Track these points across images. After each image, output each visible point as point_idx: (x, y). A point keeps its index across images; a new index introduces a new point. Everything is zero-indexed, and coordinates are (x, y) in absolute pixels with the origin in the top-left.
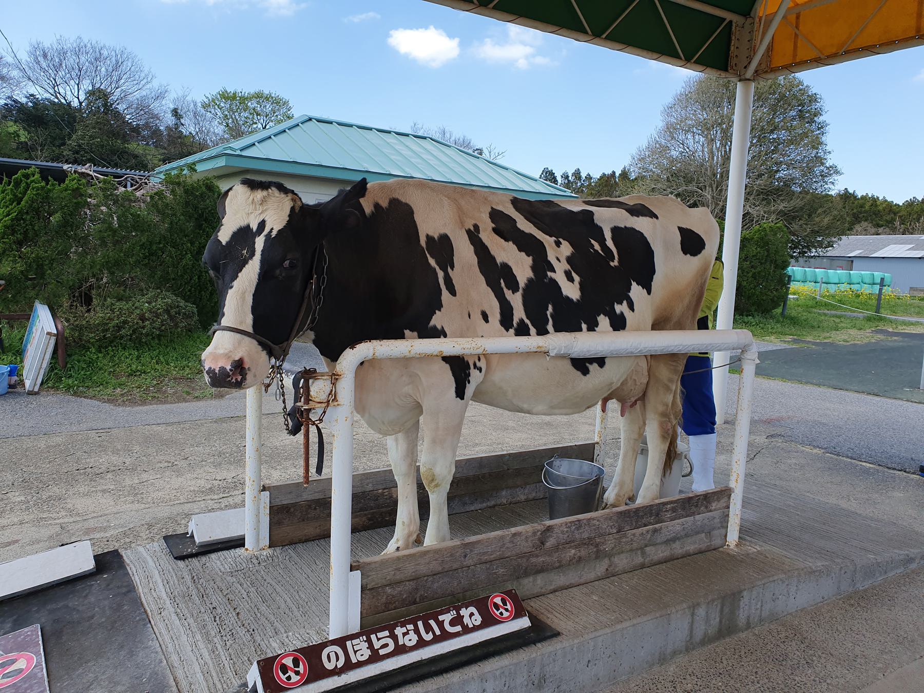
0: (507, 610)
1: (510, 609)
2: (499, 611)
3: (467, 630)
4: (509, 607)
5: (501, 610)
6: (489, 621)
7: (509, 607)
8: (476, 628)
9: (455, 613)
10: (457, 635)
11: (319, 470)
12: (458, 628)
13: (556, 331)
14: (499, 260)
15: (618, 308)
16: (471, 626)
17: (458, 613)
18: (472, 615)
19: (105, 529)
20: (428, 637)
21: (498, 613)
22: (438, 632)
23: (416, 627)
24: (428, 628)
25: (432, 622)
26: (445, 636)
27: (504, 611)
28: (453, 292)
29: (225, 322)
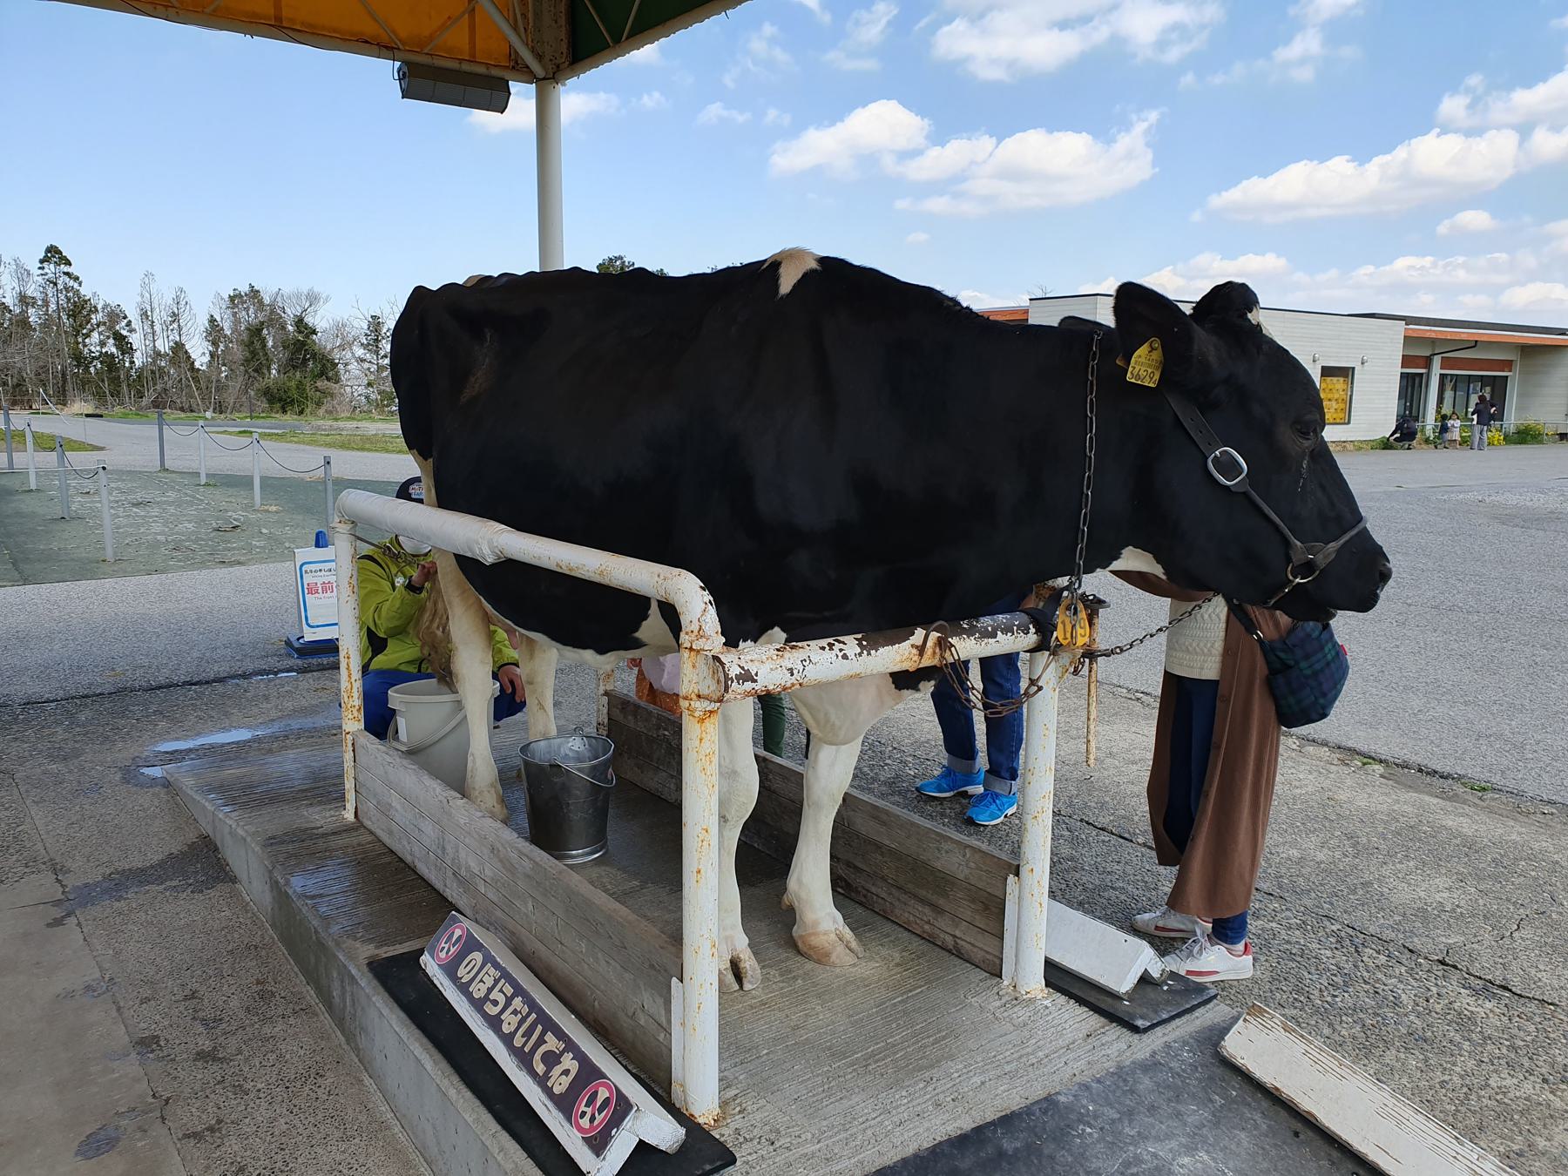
0: (592, 1119)
1: (596, 1123)
2: (585, 1109)
3: (542, 1081)
4: (599, 1118)
5: (589, 1110)
6: (565, 1103)
7: (599, 1118)
8: (548, 1092)
9: (561, 1049)
10: (532, 1072)
11: (270, 19)
12: (540, 1068)
13: (649, 599)
14: (1123, 551)
15: (865, 652)
16: (549, 1084)
17: (562, 1053)
18: (566, 1073)
19: (292, 787)
20: (518, 1041)
21: (582, 1108)
22: (527, 1049)
23: (528, 1015)
24: (528, 1034)
25: (540, 1028)
26: (525, 1060)
27: (588, 1116)
28: (701, 587)
29: (1111, 302)
